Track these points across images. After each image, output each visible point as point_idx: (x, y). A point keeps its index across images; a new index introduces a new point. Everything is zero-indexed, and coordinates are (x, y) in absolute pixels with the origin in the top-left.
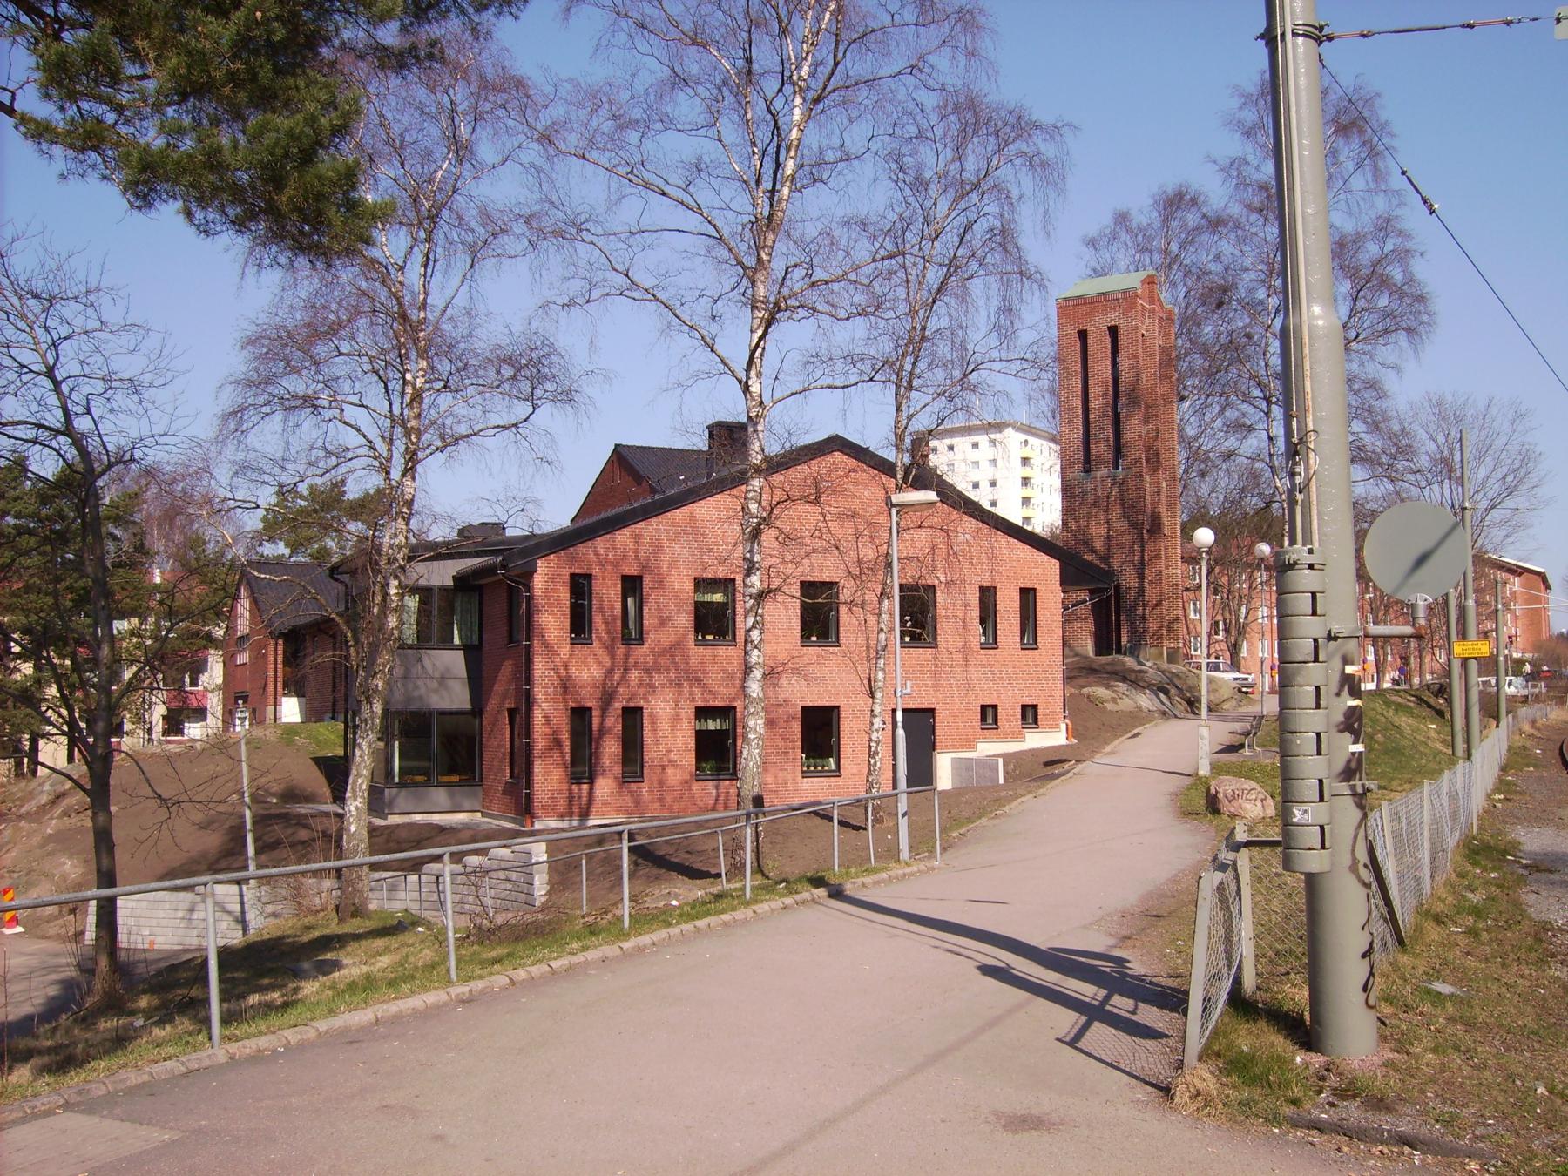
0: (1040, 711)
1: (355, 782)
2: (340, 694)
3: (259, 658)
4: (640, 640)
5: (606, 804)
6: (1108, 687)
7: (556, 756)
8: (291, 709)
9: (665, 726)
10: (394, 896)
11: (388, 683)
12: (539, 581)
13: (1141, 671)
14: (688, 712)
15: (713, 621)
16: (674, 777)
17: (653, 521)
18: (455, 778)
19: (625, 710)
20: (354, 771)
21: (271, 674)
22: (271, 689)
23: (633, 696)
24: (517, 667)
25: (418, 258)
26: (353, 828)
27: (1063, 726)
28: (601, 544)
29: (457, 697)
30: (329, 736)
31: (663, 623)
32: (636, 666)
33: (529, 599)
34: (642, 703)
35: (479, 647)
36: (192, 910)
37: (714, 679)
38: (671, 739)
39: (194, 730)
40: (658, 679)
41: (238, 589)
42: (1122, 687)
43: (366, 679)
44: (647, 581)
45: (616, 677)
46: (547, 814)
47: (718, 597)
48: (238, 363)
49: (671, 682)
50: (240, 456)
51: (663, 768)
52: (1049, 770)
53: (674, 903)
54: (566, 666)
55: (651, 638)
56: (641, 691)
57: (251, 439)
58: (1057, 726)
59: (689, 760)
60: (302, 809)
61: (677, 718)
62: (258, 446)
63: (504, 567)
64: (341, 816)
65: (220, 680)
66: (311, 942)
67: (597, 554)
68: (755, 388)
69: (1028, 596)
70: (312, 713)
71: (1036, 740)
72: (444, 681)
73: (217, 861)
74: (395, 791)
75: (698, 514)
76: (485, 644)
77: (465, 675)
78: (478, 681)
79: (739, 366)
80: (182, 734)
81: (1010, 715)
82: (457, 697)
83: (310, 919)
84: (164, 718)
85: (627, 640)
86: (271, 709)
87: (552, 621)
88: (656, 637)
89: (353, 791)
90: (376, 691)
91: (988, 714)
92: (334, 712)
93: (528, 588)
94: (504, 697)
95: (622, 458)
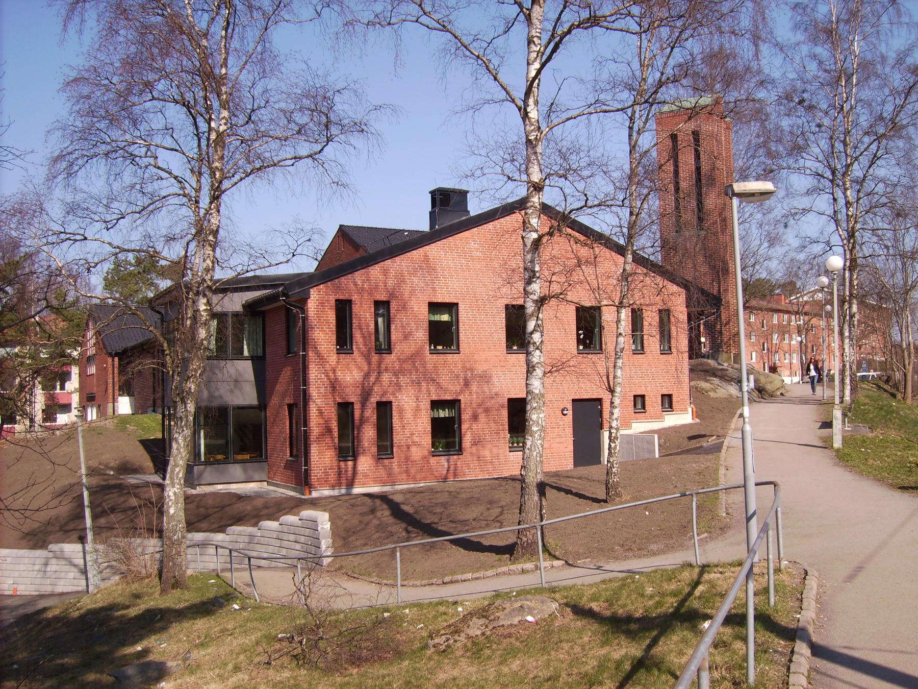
0: (674, 399)
1: (173, 471)
2: (159, 395)
3: (102, 371)
4: (389, 350)
5: (366, 476)
6: (707, 381)
7: (328, 440)
8: (124, 405)
9: (409, 415)
10: (205, 557)
11: (198, 386)
12: (312, 305)
13: (722, 370)
14: (425, 405)
15: (443, 335)
16: (417, 453)
17: (397, 259)
18: (247, 457)
19: (379, 404)
20: (172, 462)
21: (110, 381)
22: (110, 391)
23: (385, 393)
24: (295, 373)
25: (221, 22)
26: (172, 511)
27: (690, 410)
28: (358, 277)
29: (248, 396)
30: (152, 426)
31: (406, 337)
32: (386, 370)
33: (305, 320)
34: (391, 398)
35: (263, 358)
36: (46, 564)
37: (444, 379)
38: (413, 424)
39: (62, 419)
40: (403, 380)
41: (87, 324)
42: (716, 381)
43: (181, 383)
44: (393, 305)
45: (372, 379)
46: (321, 485)
47: (445, 318)
48: (60, 108)
49: (413, 382)
50: (69, 198)
51: (408, 447)
52: (694, 444)
53: (530, 618)
54: (334, 371)
55: (397, 349)
56: (391, 390)
57: (80, 181)
58: (686, 410)
59: (427, 440)
60: (132, 480)
61: (418, 409)
62: (85, 188)
63: (284, 295)
64: (161, 487)
65: (77, 386)
66: (139, 618)
67: (356, 284)
68: (533, 114)
69: (665, 315)
70: (139, 408)
71: (672, 420)
72: (237, 382)
73: (66, 524)
74: (202, 467)
75: (429, 253)
76: (268, 356)
77: (252, 378)
78: (263, 384)
79: (519, 95)
80: (55, 420)
81: (654, 403)
82: (248, 396)
83: (135, 587)
84: (43, 411)
85: (379, 350)
86: (110, 405)
87: (323, 335)
88: (401, 348)
89: (172, 478)
90: (189, 392)
91: (640, 401)
92: (154, 406)
93: (303, 310)
94: (284, 396)
95: (344, 233)
